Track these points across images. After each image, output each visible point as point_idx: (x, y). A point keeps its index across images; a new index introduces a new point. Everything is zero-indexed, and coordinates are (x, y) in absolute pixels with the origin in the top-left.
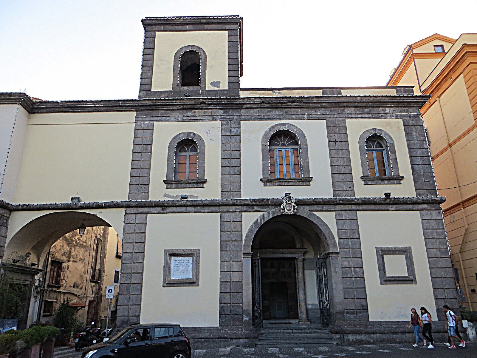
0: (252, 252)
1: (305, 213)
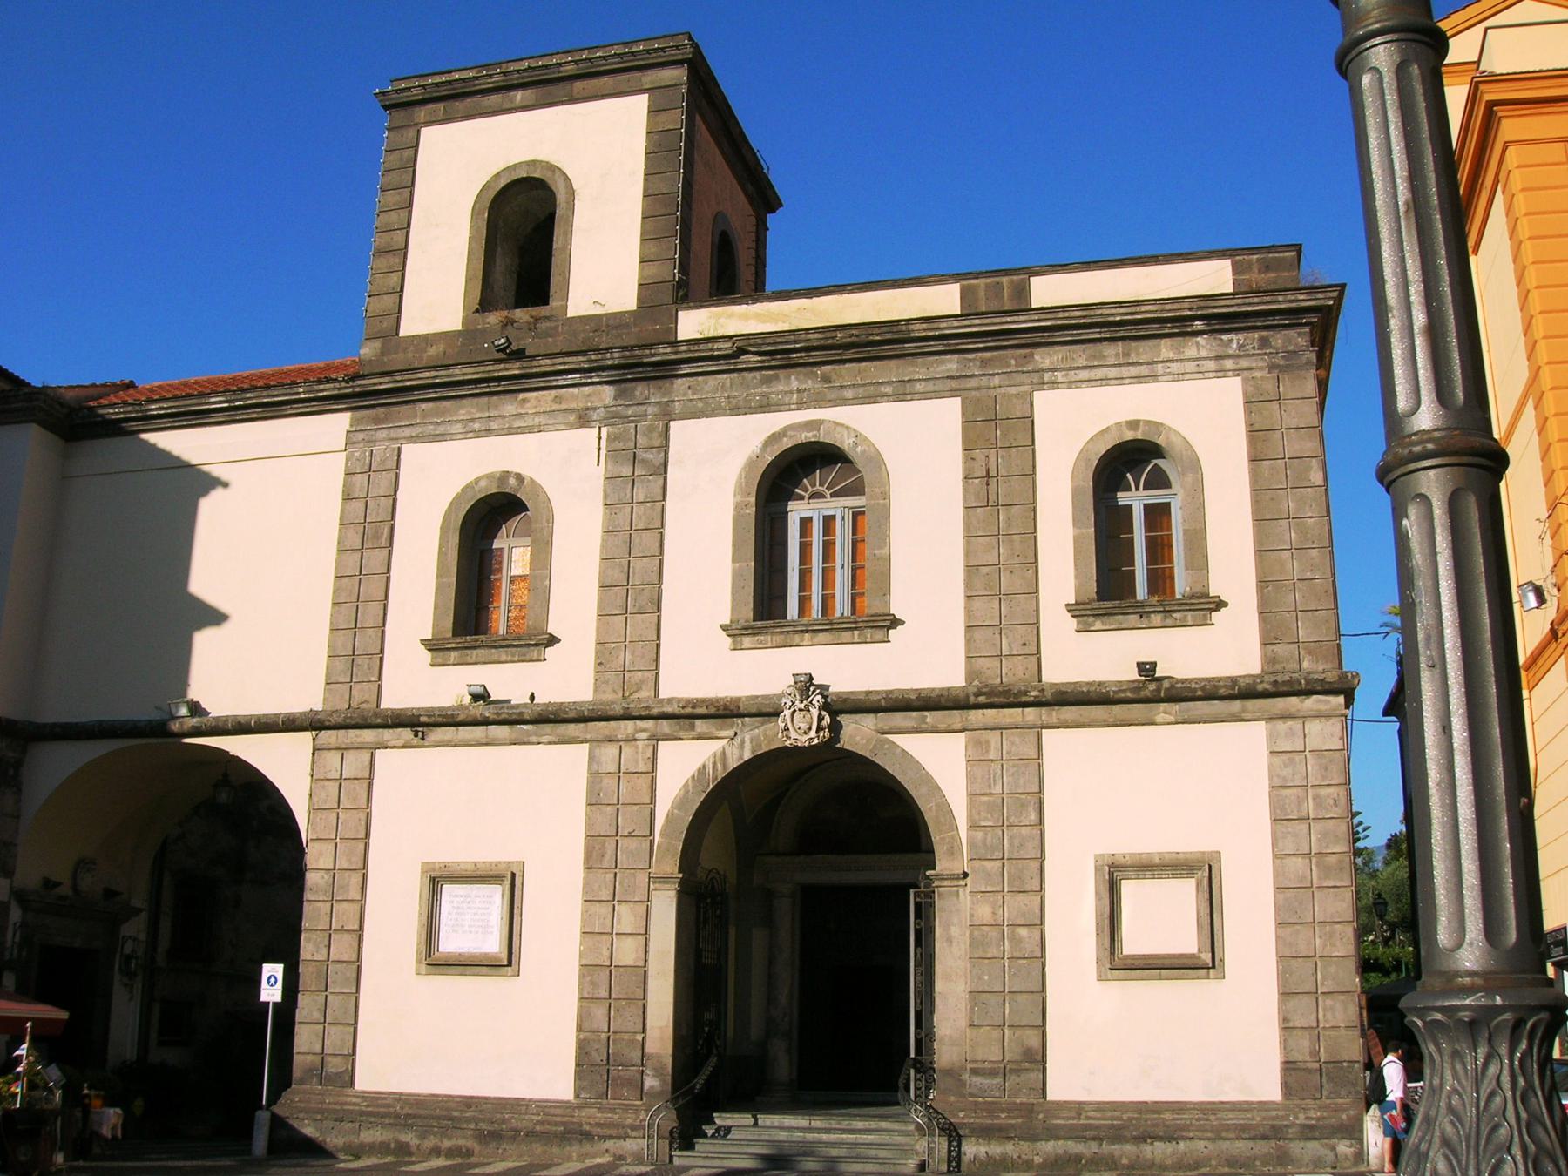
0: (679, 872)
1: (862, 739)
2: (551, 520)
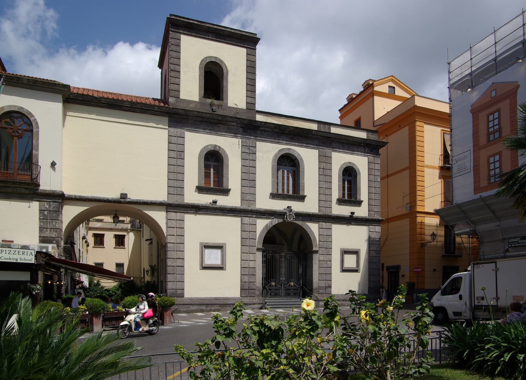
2: (228, 160)
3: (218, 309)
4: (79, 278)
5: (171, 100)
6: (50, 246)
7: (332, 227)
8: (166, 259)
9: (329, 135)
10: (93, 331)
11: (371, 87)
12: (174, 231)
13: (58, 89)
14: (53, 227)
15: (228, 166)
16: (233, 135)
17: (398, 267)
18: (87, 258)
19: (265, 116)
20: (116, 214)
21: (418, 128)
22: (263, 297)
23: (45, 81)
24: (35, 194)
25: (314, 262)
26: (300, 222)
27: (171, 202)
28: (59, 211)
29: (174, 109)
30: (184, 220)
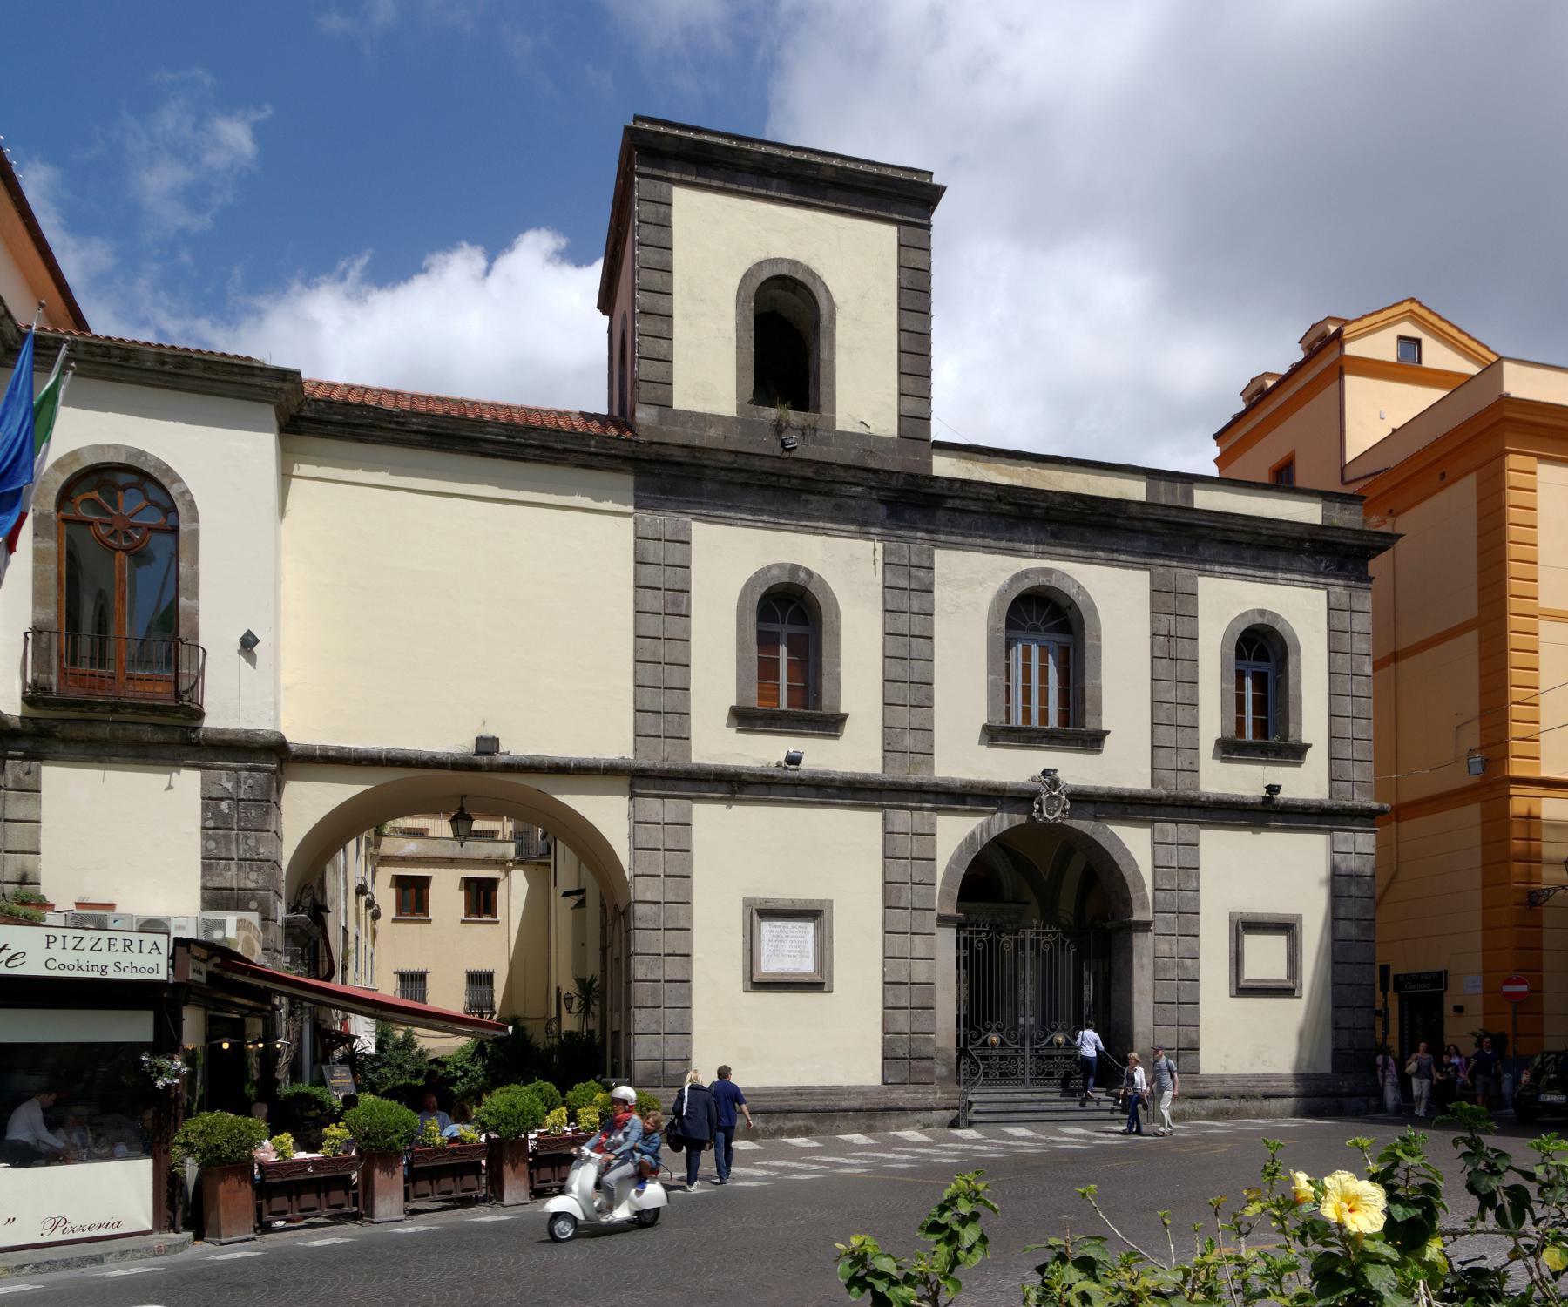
2: (838, 616)
3: (805, 1126)
4: (342, 1024)
5: (644, 415)
6: (232, 919)
7: (1198, 836)
8: (629, 957)
9: (1187, 515)
10: (372, 1217)
11: (1335, 342)
12: (657, 863)
13: (261, 387)
14: (248, 856)
15: (838, 635)
16: (852, 528)
17: (1438, 980)
18: (375, 957)
19: (965, 459)
20: (462, 809)
21: (1513, 478)
22: (958, 1083)
23: (216, 359)
24: (188, 743)
25: (1135, 960)
26: (1086, 823)
27: (645, 763)
28: (268, 801)
29: (654, 446)
30: (689, 825)
